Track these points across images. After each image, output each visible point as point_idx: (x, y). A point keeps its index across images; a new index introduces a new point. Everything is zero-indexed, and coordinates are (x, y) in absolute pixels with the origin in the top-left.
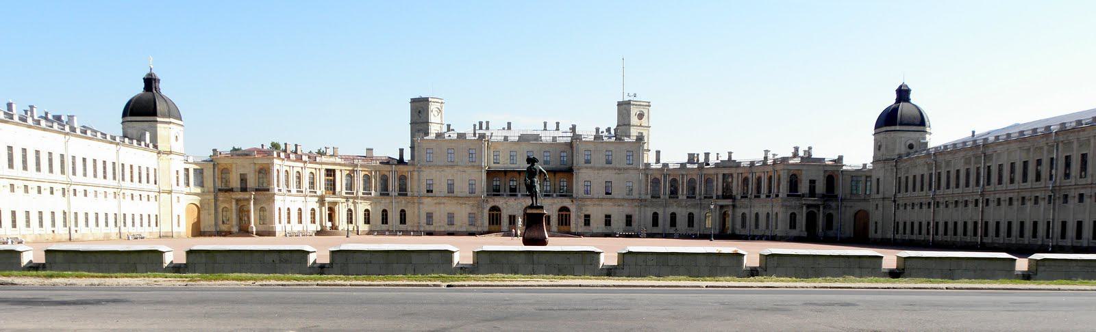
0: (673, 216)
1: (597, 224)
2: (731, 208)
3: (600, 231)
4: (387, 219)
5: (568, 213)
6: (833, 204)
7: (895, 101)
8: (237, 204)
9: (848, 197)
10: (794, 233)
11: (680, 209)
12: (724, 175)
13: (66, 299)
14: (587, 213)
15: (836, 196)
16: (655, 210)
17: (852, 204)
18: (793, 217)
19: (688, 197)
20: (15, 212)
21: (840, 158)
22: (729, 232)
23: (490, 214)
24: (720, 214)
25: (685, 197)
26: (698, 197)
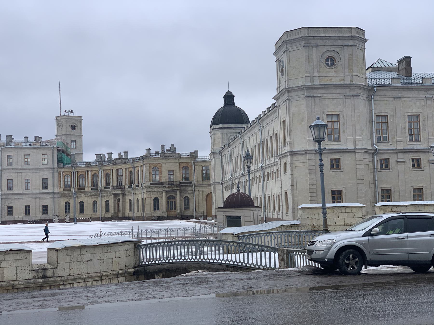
0: (82, 204)
1: (19, 213)
2: (121, 196)
3: (38, 219)
4: (158, 205)
5: (173, 200)
6: (189, 189)
7: (223, 105)
8: (166, 195)
9: (200, 183)
10: (157, 214)
11: (86, 198)
12: (117, 170)
13: (380, 277)
14: (10, 205)
15: (191, 183)
16: (67, 200)
17: (203, 188)
18: (156, 202)
19: (92, 189)
20: (29, 207)
21: (197, 151)
22: (120, 215)
23: (168, 202)
24: (114, 201)
25: (90, 189)
26: (99, 189)
